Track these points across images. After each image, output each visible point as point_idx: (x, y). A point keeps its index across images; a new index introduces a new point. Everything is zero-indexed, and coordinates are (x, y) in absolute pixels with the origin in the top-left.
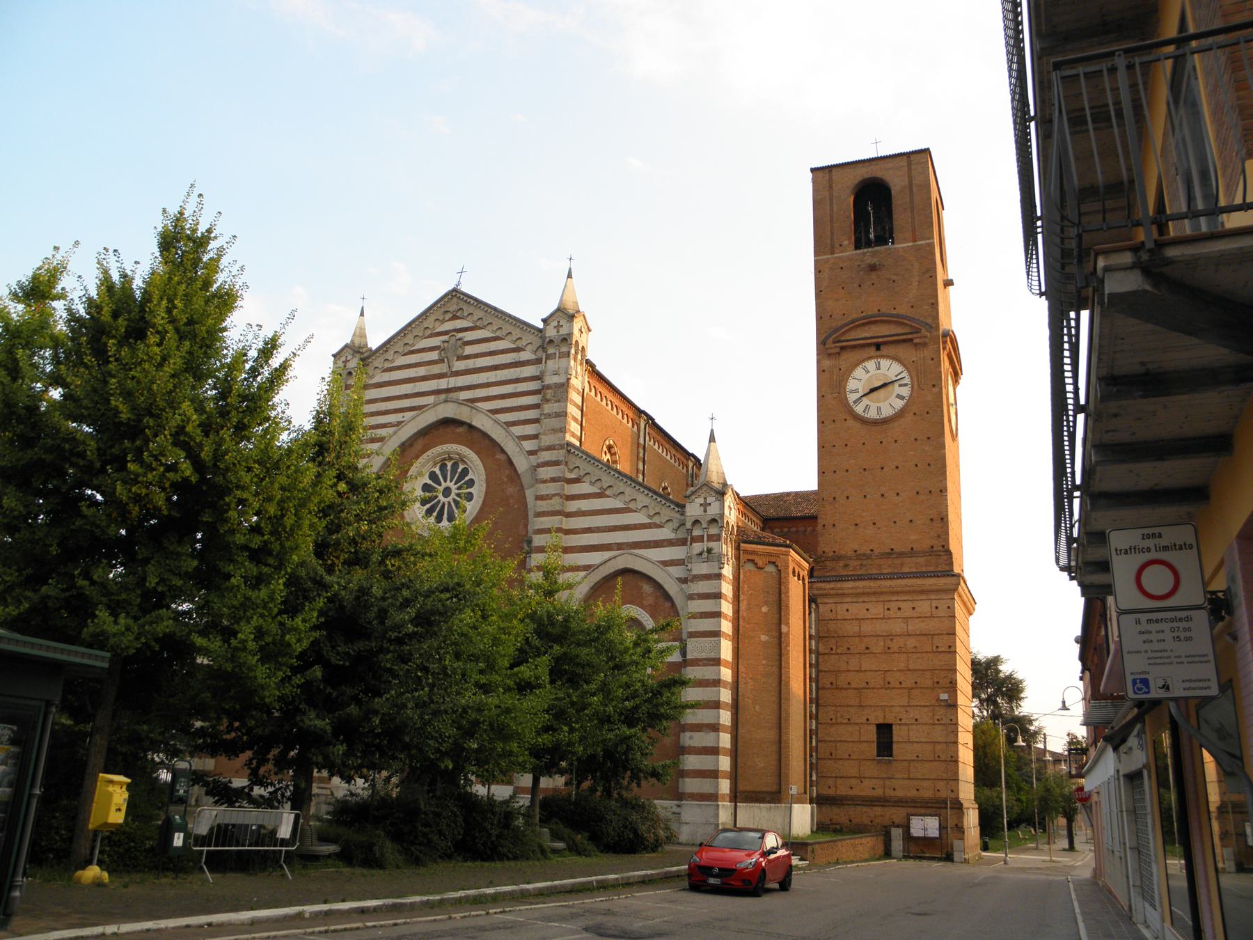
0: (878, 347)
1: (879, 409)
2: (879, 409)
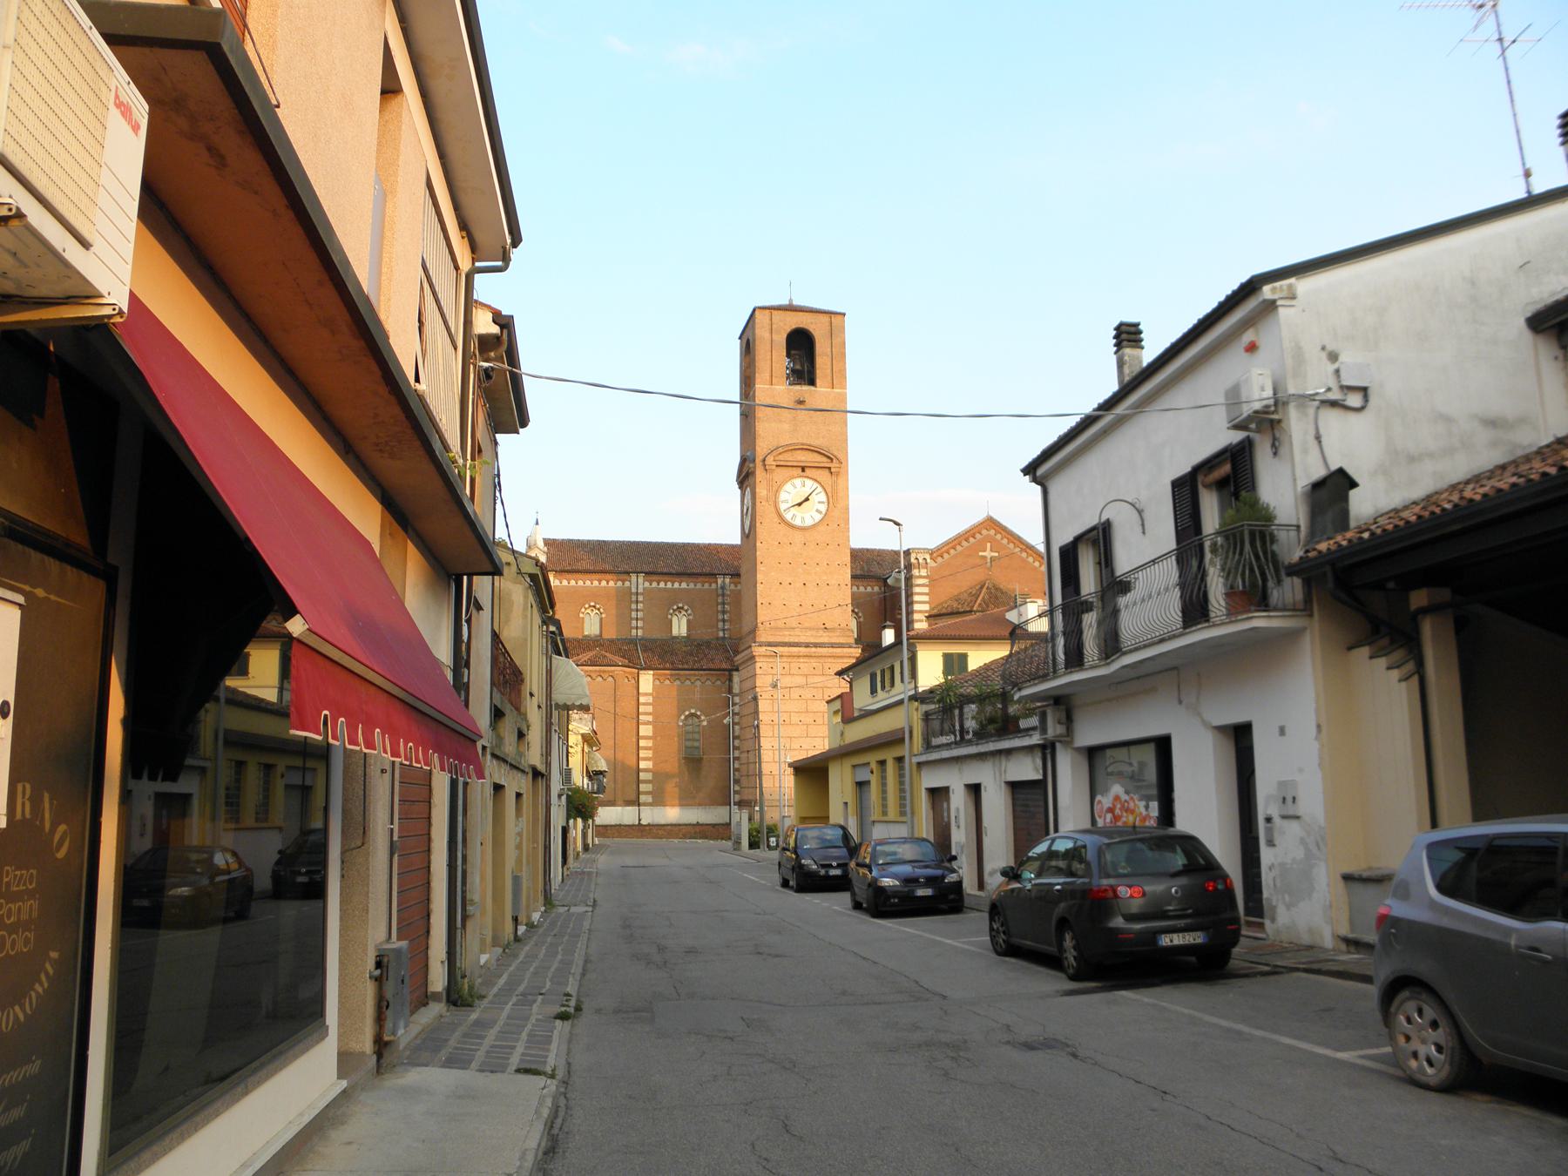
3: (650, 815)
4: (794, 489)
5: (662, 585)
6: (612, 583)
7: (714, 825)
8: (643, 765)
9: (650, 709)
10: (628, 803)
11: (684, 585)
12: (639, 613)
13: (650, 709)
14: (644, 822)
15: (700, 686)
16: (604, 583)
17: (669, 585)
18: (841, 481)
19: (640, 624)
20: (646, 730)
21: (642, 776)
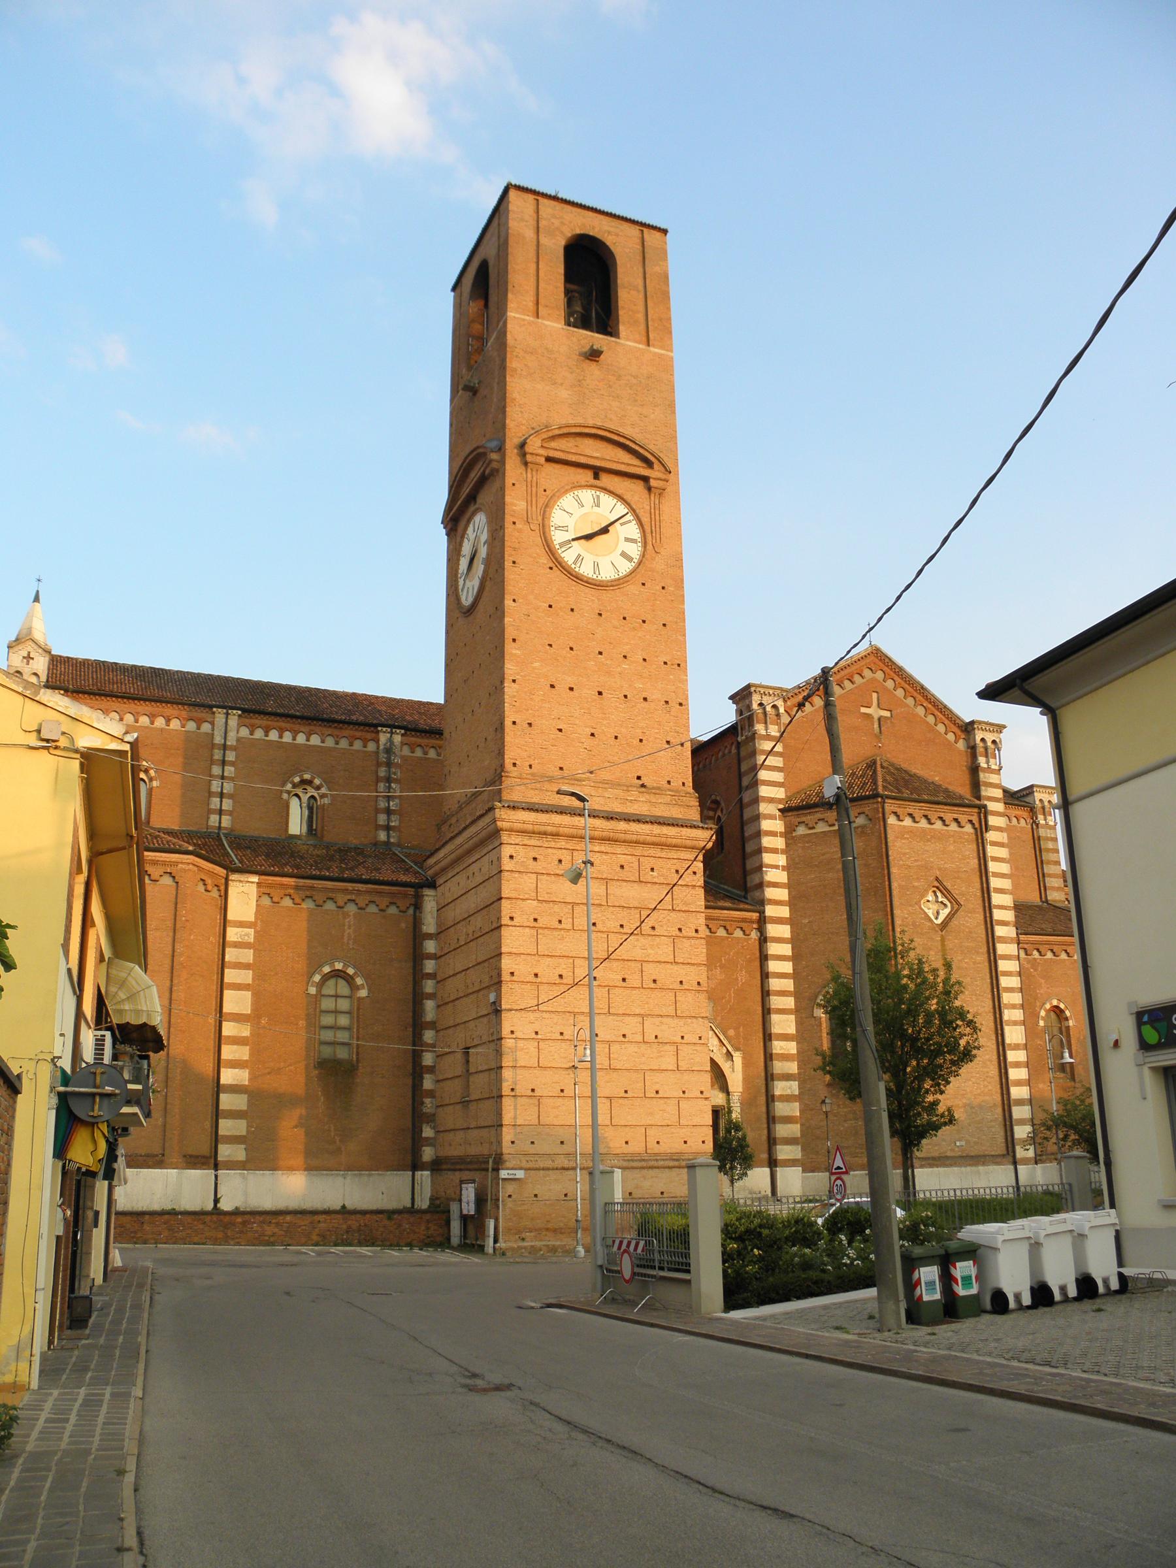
0: (597, 472)
1: (596, 565)
2: (596, 565)
3: (242, 1190)
4: (577, 509)
5: (273, 735)
6: (175, 724)
7: (390, 1214)
8: (228, 1076)
9: (248, 956)
10: (194, 1161)
11: (315, 740)
12: (225, 782)
13: (248, 956)
14: (226, 1205)
15: (355, 915)
16: (160, 722)
17: (287, 737)
18: (666, 507)
19: (227, 804)
20: (236, 1002)
21: (226, 1101)
